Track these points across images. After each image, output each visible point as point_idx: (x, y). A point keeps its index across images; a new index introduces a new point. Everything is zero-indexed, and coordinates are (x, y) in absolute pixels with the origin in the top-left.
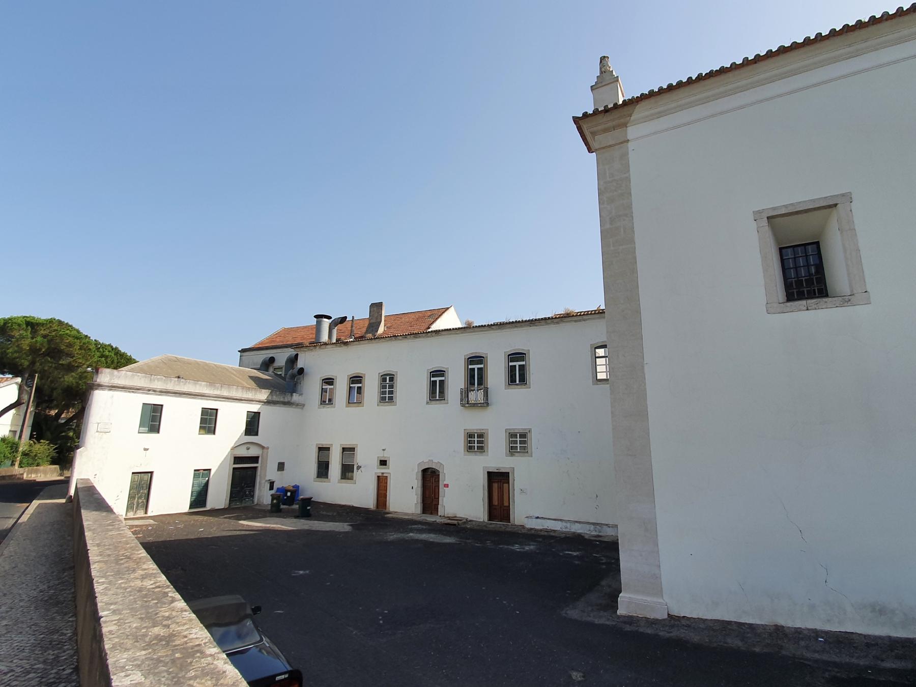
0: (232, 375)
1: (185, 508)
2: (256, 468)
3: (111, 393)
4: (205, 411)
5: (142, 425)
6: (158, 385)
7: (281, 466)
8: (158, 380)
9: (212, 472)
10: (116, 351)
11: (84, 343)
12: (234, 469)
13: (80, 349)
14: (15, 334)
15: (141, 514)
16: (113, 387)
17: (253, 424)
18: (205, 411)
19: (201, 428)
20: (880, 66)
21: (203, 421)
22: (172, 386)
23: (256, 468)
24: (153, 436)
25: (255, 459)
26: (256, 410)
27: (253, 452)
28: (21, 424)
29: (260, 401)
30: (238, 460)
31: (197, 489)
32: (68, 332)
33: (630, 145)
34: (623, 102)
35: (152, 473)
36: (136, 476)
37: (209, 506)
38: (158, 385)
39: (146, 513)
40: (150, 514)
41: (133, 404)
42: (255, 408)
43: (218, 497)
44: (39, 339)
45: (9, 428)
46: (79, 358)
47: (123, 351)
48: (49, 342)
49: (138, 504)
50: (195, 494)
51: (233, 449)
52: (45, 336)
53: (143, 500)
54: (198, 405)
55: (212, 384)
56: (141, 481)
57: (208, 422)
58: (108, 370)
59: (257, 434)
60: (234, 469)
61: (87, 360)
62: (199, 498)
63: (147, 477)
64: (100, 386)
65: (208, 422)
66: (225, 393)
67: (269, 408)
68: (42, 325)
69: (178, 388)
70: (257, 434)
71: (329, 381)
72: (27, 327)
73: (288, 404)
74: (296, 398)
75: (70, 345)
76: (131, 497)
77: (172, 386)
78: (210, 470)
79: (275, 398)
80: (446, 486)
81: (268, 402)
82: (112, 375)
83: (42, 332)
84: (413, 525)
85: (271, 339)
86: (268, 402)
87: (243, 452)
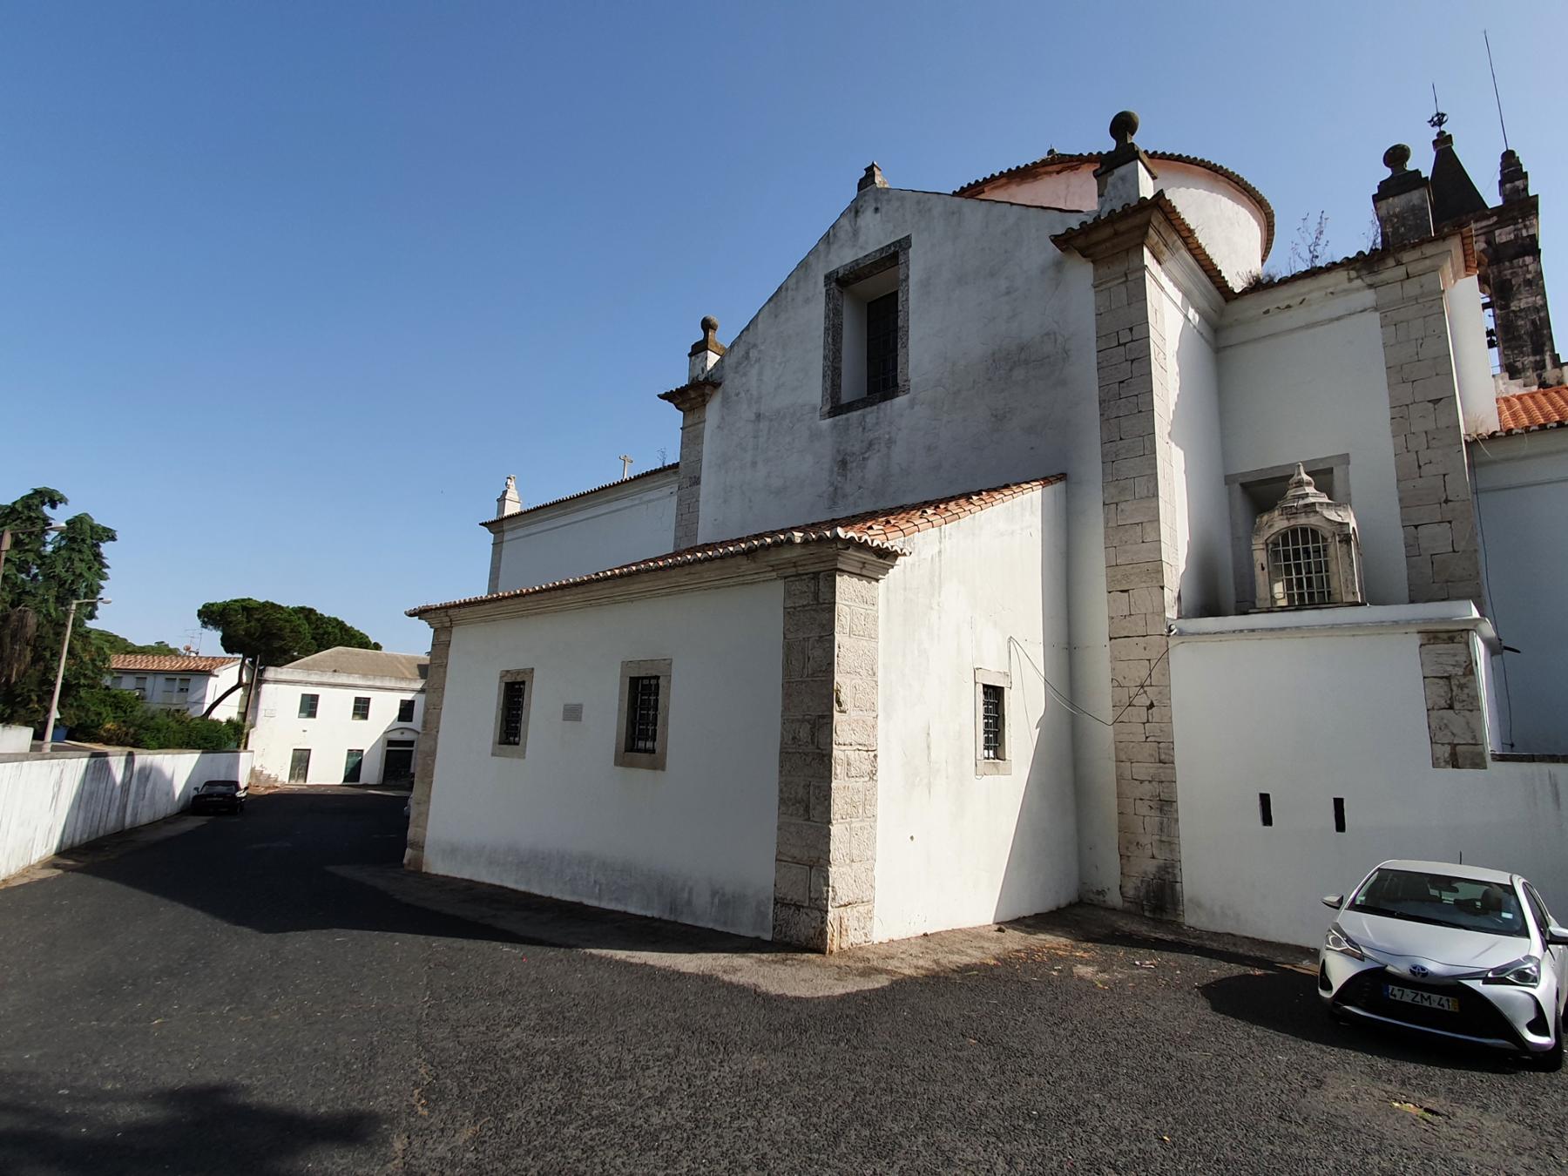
0: (400, 666)
1: (340, 781)
2: (412, 751)
3: (276, 686)
4: (358, 700)
5: (301, 712)
6: (315, 678)
8: (316, 674)
9: (365, 753)
10: (340, 625)
11: (295, 626)
12: (388, 751)
13: (291, 632)
15: (301, 782)
16: (276, 682)
17: (406, 710)
18: (358, 700)
19: (354, 714)
20: (599, 516)
21: (367, 709)
23: (412, 751)
24: (311, 720)
25: (411, 743)
26: (409, 699)
27: (408, 736)
28: (245, 704)
29: (413, 691)
30: (391, 743)
31: (351, 766)
32: (279, 615)
33: (504, 544)
35: (310, 750)
36: (297, 752)
37: (361, 782)
38: (315, 678)
39: (305, 781)
40: (308, 783)
41: (293, 695)
42: (409, 696)
43: (371, 772)
44: (253, 624)
45: (237, 710)
46: (290, 642)
47: (349, 625)
48: (263, 626)
49: (299, 774)
50: (349, 770)
51: (385, 733)
52: (259, 620)
53: (302, 771)
55: (365, 675)
56: (301, 756)
57: (361, 708)
58: (273, 668)
59: (411, 721)
60: (388, 751)
61: (297, 643)
62: (353, 773)
63: (306, 753)
64: (266, 681)
65: (361, 708)
66: (378, 683)
67: (423, 697)
68: (257, 609)
69: (332, 681)
70: (411, 721)
72: (243, 611)
75: (281, 629)
76: (293, 768)
78: (362, 751)
82: (276, 671)
83: (256, 616)
84: (1172, 941)
87: (396, 736)
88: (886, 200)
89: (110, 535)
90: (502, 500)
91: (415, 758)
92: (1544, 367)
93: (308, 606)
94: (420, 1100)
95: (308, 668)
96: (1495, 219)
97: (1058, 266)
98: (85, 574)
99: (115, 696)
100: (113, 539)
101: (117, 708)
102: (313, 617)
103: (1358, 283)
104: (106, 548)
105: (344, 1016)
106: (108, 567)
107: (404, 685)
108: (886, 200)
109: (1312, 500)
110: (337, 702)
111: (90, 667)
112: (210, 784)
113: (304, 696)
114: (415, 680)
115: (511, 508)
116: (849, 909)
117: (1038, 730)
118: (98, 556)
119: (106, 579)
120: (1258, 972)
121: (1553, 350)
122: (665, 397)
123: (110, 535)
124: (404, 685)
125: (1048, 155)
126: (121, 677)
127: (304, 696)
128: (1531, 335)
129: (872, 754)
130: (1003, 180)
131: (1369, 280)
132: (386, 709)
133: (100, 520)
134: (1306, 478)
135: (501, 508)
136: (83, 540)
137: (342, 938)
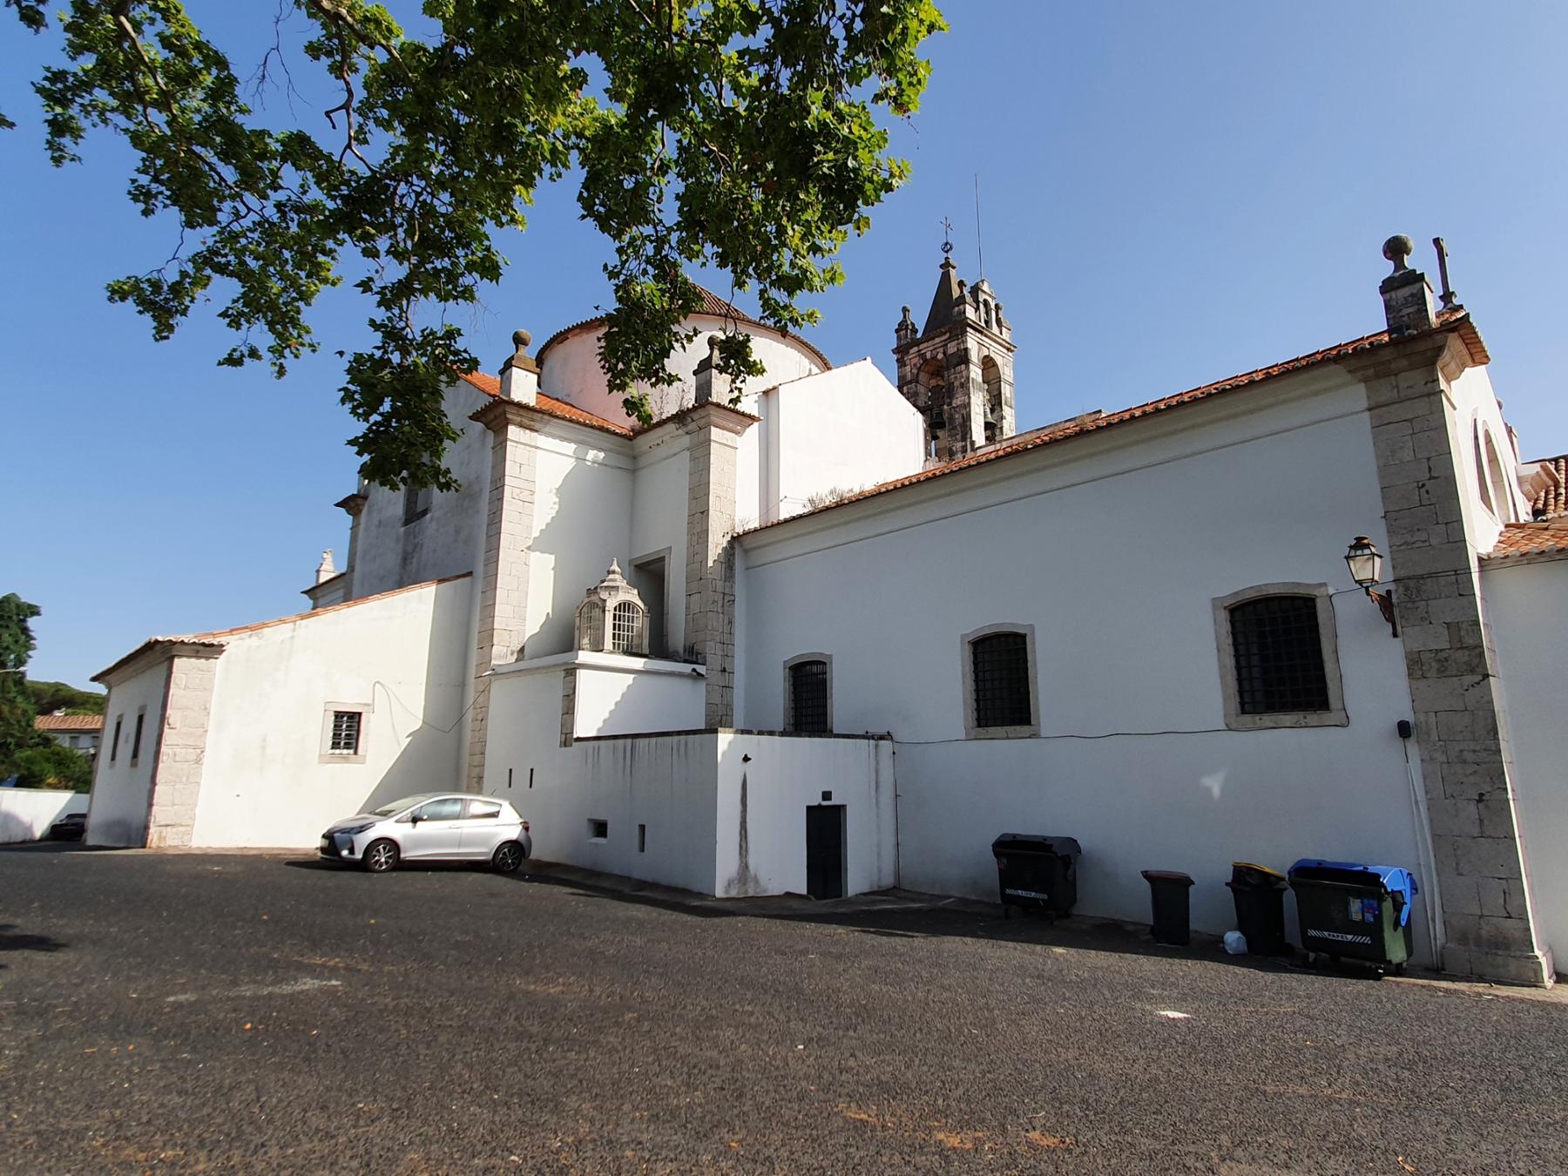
4: (830, 799)
18: (830, 799)
89: (34, 611)
92: (966, 451)
96: (948, 335)
97: (485, 431)
98: (12, 647)
99: (58, 754)
100: (38, 614)
101: (60, 764)
103: (680, 432)
104: (32, 623)
105: (78, 969)
106: (34, 639)
109: (618, 584)
111: (16, 727)
112: (70, 816)
115: (324, 578)
116: (169, 828)
117: (409, 739)
118: (25, 630)
119: (34, 649)
121: (971, 438)
122: (338, 505)
123: (34, 611)
126: (77, 738)
128: (961, 425)
129: (199, 751)
130: (577, 331)
131: (685, 429)
133: (26, 598)
134: (617, 569)
136: (10, 617)
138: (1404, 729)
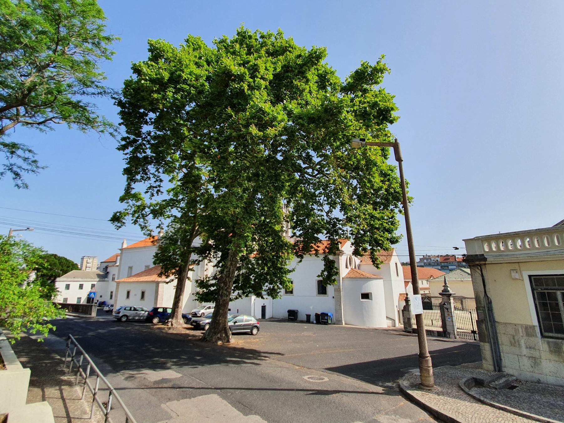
4: (80, 285)
6: (69, 280)
7: (101, 296)
14: (169, 170)
16: (59, 281)
17: (93, 286)
18: (80, 285)
21: (80, 287)
22: (72, 280)
24: (68, 290)
34: (134, 194)
38: (69, 280)
54: (79, 283)
55: (82, 278)
57: (81, 287)
65: (81, 287)
66: (85, 280)
71: (114, 275)
73: (104, 281)
74: (106, 279)
77: (72, 280)
79: (101, 280)
80: (230, 310)
81: (99, 281)
85: (108, 259)
86: (99, 281)
88: (185, 68)
90: (123, 244)
91: (235, 367)
93: (54, 254)
94: (389, 225)
95: (67, 277)
102: (57, 257)
107: (92, 280)
108: (185, 68)
110: (74, 286)
113: (66, 285)
114: (95, 278)
120: (100, 331)
124: (92, 280)
125: (249, 36)
127: (66, 285)
132: (87, 288)
135: (122, 246)
137: (392, 356)
138: (333, 297)
